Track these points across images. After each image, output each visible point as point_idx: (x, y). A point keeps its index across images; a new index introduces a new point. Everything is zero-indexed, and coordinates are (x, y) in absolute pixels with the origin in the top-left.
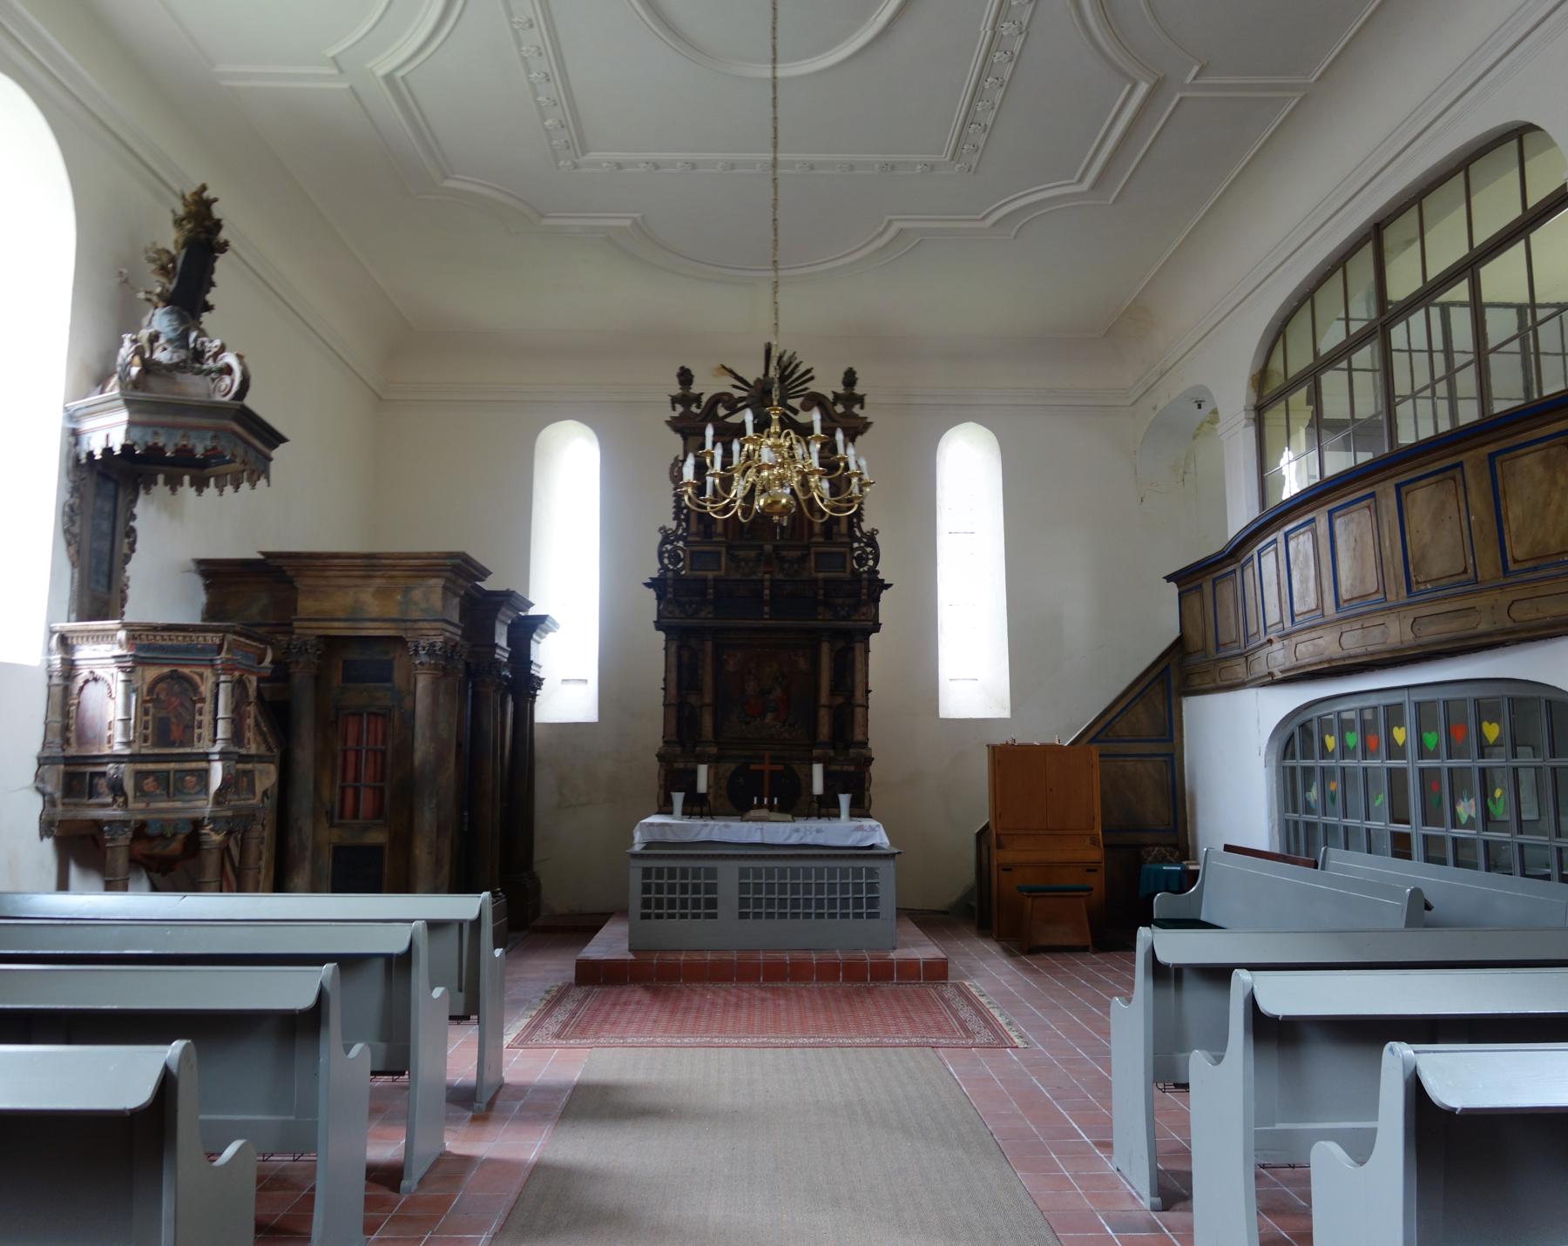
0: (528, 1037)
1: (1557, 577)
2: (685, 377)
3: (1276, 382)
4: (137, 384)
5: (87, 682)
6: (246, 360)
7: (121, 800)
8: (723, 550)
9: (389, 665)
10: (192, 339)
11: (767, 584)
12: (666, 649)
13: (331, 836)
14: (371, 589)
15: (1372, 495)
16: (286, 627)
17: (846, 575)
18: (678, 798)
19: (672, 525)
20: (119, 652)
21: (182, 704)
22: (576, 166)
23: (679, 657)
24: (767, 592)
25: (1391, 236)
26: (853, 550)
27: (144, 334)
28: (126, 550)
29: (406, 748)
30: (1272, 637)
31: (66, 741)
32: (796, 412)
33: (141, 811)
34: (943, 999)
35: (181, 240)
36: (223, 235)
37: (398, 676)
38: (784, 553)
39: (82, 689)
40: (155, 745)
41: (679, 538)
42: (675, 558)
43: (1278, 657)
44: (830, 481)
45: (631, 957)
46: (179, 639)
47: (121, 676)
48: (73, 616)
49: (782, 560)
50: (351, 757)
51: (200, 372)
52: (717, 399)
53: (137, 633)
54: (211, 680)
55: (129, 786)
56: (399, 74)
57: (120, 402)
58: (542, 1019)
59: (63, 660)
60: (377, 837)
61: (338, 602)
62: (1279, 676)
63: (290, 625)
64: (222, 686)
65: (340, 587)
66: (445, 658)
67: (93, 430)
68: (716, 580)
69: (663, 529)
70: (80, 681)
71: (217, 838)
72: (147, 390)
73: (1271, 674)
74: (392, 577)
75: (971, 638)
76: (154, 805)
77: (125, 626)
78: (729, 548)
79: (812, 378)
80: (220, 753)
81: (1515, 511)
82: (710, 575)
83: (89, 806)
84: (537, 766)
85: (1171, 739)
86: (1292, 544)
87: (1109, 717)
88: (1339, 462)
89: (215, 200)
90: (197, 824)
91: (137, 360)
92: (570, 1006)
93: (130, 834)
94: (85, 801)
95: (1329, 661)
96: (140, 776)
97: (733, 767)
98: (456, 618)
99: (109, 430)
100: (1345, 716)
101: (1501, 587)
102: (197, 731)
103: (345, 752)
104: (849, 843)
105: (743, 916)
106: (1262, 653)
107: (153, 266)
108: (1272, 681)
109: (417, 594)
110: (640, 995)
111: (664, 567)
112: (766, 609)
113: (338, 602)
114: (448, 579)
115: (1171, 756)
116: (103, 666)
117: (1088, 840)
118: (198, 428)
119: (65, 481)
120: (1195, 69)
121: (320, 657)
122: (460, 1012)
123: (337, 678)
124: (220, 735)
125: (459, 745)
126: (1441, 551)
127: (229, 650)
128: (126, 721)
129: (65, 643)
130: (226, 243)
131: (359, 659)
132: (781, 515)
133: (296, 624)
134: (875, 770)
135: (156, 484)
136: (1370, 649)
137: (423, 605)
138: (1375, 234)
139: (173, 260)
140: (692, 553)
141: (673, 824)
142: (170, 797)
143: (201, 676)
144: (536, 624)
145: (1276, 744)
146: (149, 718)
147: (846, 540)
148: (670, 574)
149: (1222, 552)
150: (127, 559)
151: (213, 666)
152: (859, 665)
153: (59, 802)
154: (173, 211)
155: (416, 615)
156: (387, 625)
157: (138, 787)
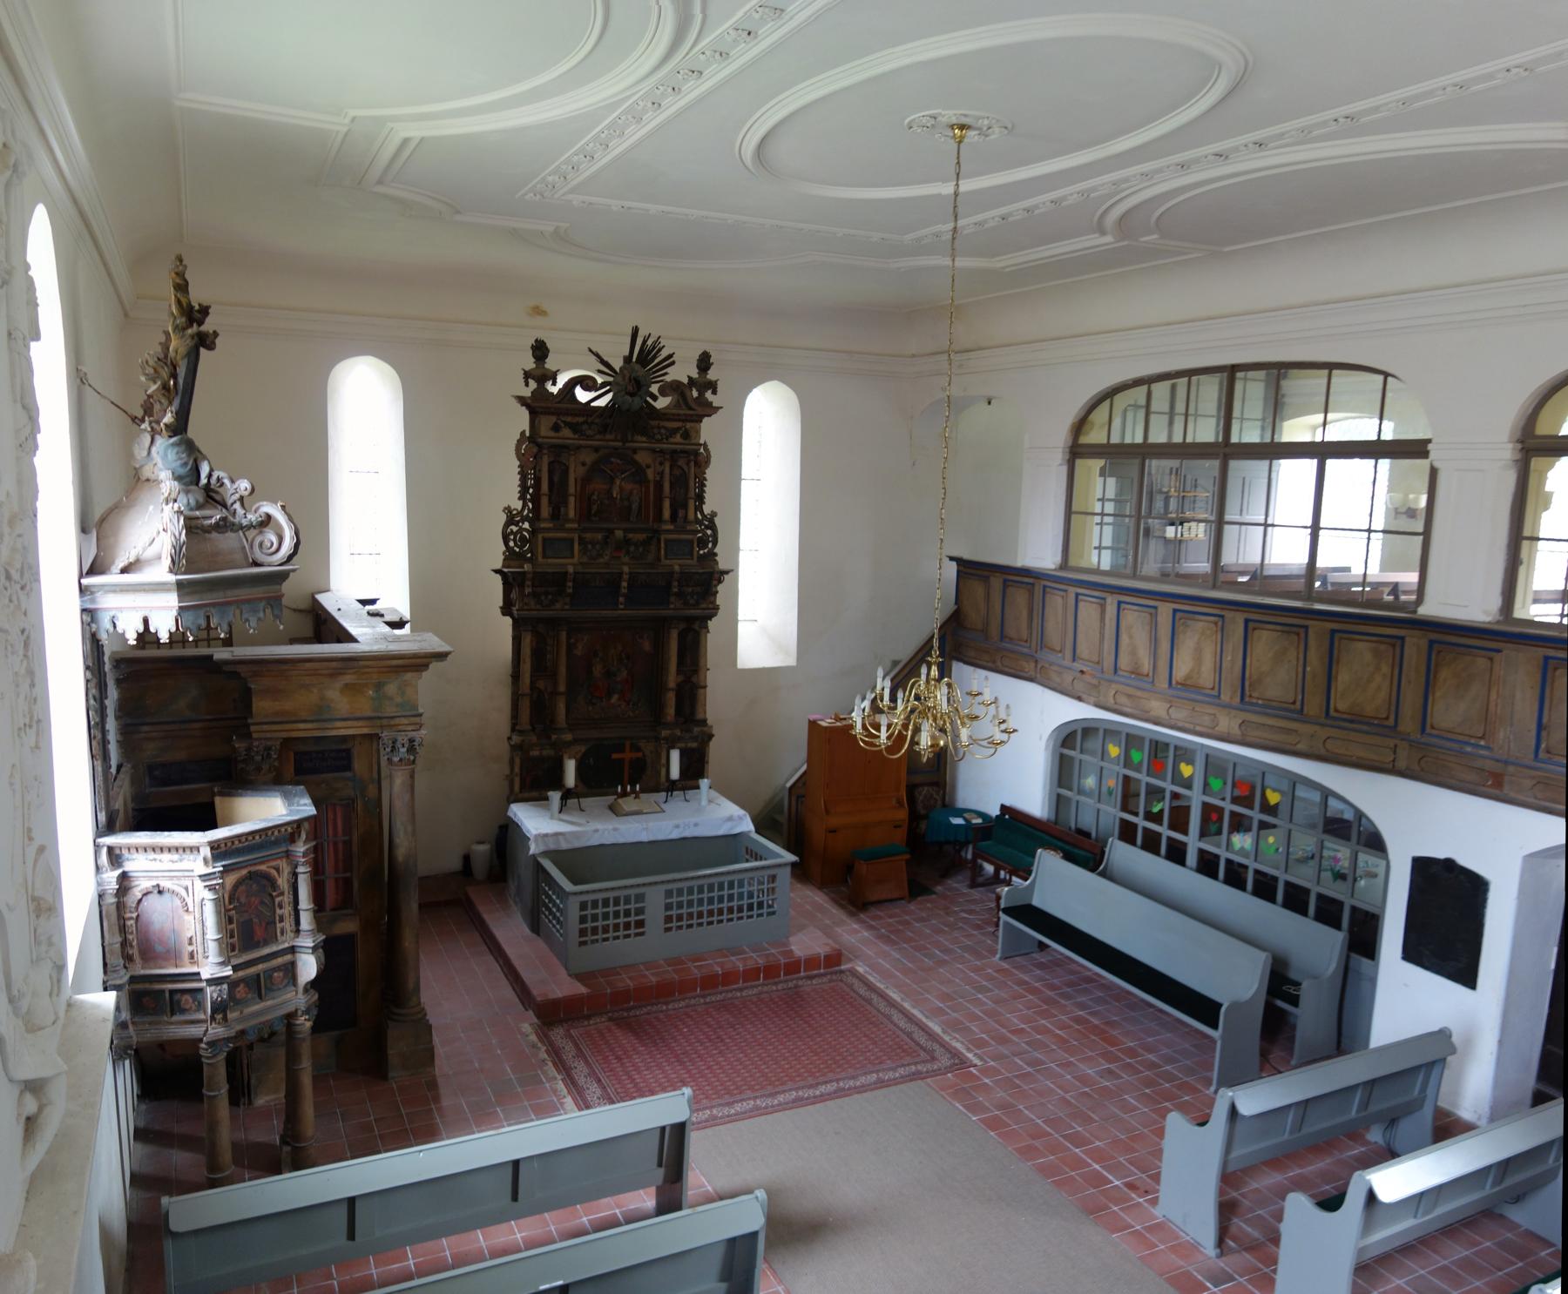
1: (1367, 733)
10: (204, 474)
11: (626, 577)
19: (518, 505)
24: (625, 584)
31: (128, 958)
32: (655, 398)
54: (286, 870)
63: (248, 726)
69: (508, 510)
81: (1343, 677)
90: (291, 1016)
97: (583, 749)
101: (1322, 725)
104: (721, 832)
105: (668, 930)
117: (894, 801)
126: (1278, 683)
129: (115, 857)
133: (252, 728)
134: (713, 744)
137: (399, 700)
146: (234, 926)
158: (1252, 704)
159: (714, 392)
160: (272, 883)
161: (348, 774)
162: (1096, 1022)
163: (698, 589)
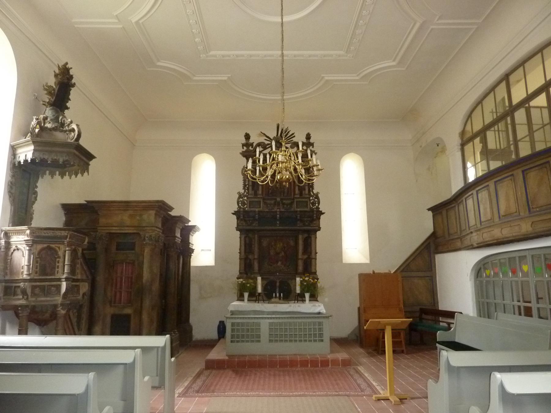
0: (186, 392)
2: (247, 136)
3: (468, 135)
4: (38, 135)
5: (14, 250)
6: (80, 127)
7: (26, 297)
8: (262, 200)
9: (133, 244)
11: (278, 213)
12: (240, 238)
13: (110, 311)
15: (512, 175)
16: (95, 230)
17: (308, 209)
18: (246, 295)
19: (242, 191)
20: (27, 238)
22: (207, 57)
23: (245, 241)
24: (278, 216)
25: (512, 78)
26: (310, 200)
27: (42, 116)
29: (140, 276)
30: (472, 231)
33: (34, 301)
34: (350, 374)
35: (57, 83)
36: (73, 81)
38: (284, 201)
39: (12, 253)
40: (40, 275)
41: (245, 196)
42: (243, 204)
43: (475, 238)
44: (305, 169)
45: (227, 358)
46: (50, 234)
47: (27, 248)
48: (10, 225)
49: (283, 204)
51: (62, 131)
52: (259, 145)
53: (34, 232)
55: (29, 291)
56: (141, 22)
57: (31, 142)
58: (192, 385)
62: (476, 246)
64: (67, 252)
67: (21, 153)
68: (259, 211)
69: (239, 193)
70: (12, 250)
71: (63, 312)
72: (41, 138)
73: (472, 245)
75: (355, 233)
77: (29, 228)
78: (264, 199)
79: (294, 136)
82: (257, 210)
85: (432, 270)
86: (480, 195)
87: (407, 263)
88: (495, 165)
89: (71, 68)
90: (56, 306)
91: (38, 126)
92: (203, 378)
93: (29, 311)
94: (12, 297)
95: (497, 240)
96: (34, 288)
98: (160, 225)
99: (26, 153)
100: (502, 261)
102: (57, 269)
105: (270, 341)
106: (468, 237)
107: (46, 92)
108: (471, 247)
110: (230, 373)
111: (239, 207)
112: (278, 222)
114: (157, 211)
115: (432, 277)
116: (21, 244)
119: (10, 172)
120: (438, 17)
122: (157, 384)
123: (114, 248)
124: (66, 271)
125: (161, 275)
127: (70, 238)
128: (28, 266)
130: (75, 84)
131: (124, 242)
132: (286, 182)
133: (99, 228)
136: (514, 234)
138: (506, 78)
139: (54, 90)
140: (250, 201)
141: (245, 305)
142: (46, 296)
143: (59, 248)
145: (474, 272)
147: (308, 196)
148: (242, 210)
149: (450, 199)
152: (313, 243)
154: (55, 72)
155: (144, 225)
156: (131, 228)
157: (33, 292)
158: (534, 212)
159: (313, 147)
160: (56, 252)
161: (133, 252)
163: (309, 219)
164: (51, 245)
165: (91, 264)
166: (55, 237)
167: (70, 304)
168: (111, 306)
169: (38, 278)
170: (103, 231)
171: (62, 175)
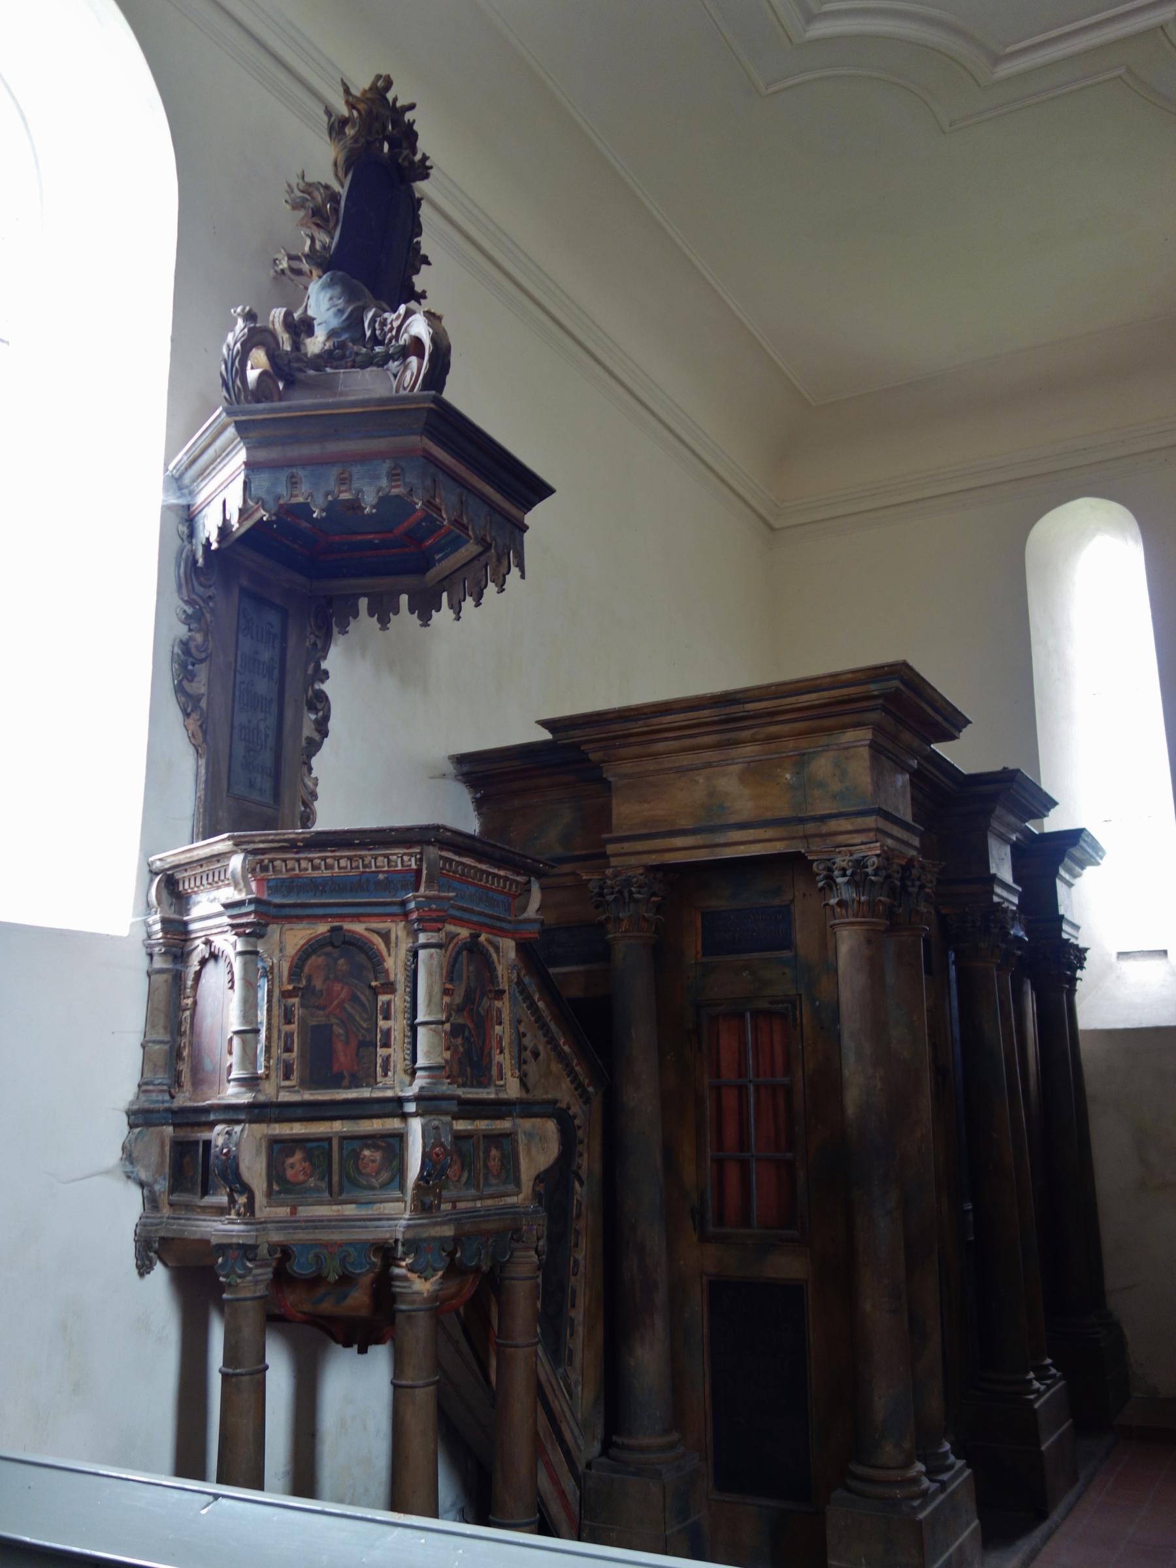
4: (263, 391)
5: (203, 962)
7: (242, 1200)
14: (735, 769)
21: (354, 998)
28: (308, 730)
29: (828, 1080)
37: (804, 938)
39: (198, 975)
50: (730, 1100)
54: (405, 945)
59: (165, 921)
60: (787, 1266)
61: (681, 799)
65: (682, 771)
66: (890, 895)
71: (422, 1286)
72: (272, 396)
74: (770, 739)
76: (306, 1212)
80: (417, 1099)
83: (205, 1209)
84: (1093, 1109)
90: (386, 1252)
96: (278, 1149)
98: (905, 812)
102: (381, 1052)
103: (717, 1089)
109: (822, 766)
113: (681, 799)
114: (878, 728)
118: (363, 458)
119: (176, 603)
121: (659, 908)
123: (693, 946)
131: (728, 904)
133: (611, 849)
135: (356, 615)
137: (836, 787)
139: (334, 198)
142: (335, 1196)
143: (385, 936)
144: (1070, 847)
146: (294, 1027)
150: (314, 747)
151: (406, 915)
153: (164, 1200)
154: (328, 113)
157: (275, 1173)
160: (376, 961)
161: (786, 954)
162: (469, 1070)
164: (348, 926)
165: (588, 1027)
166: (363, 883)
167: (457, 1240)
168: (704, 1239)
169: (295, 1098)
170: (633, 861)
171: (425, 607)
